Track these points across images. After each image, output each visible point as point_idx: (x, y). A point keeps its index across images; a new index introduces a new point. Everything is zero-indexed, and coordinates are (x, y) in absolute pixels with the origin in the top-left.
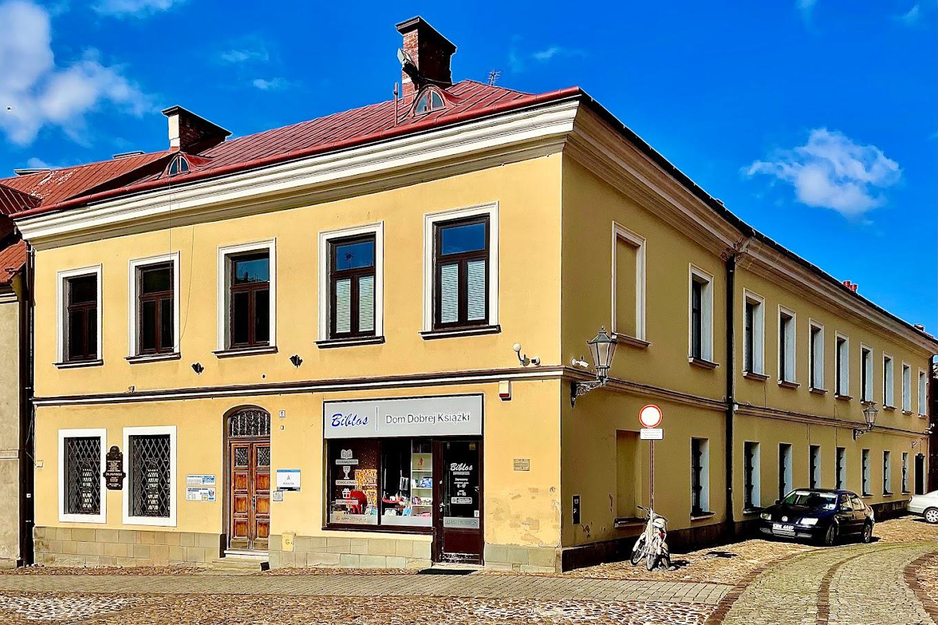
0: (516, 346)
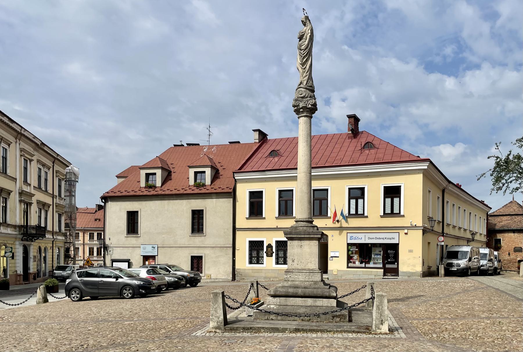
0: (411, 221)
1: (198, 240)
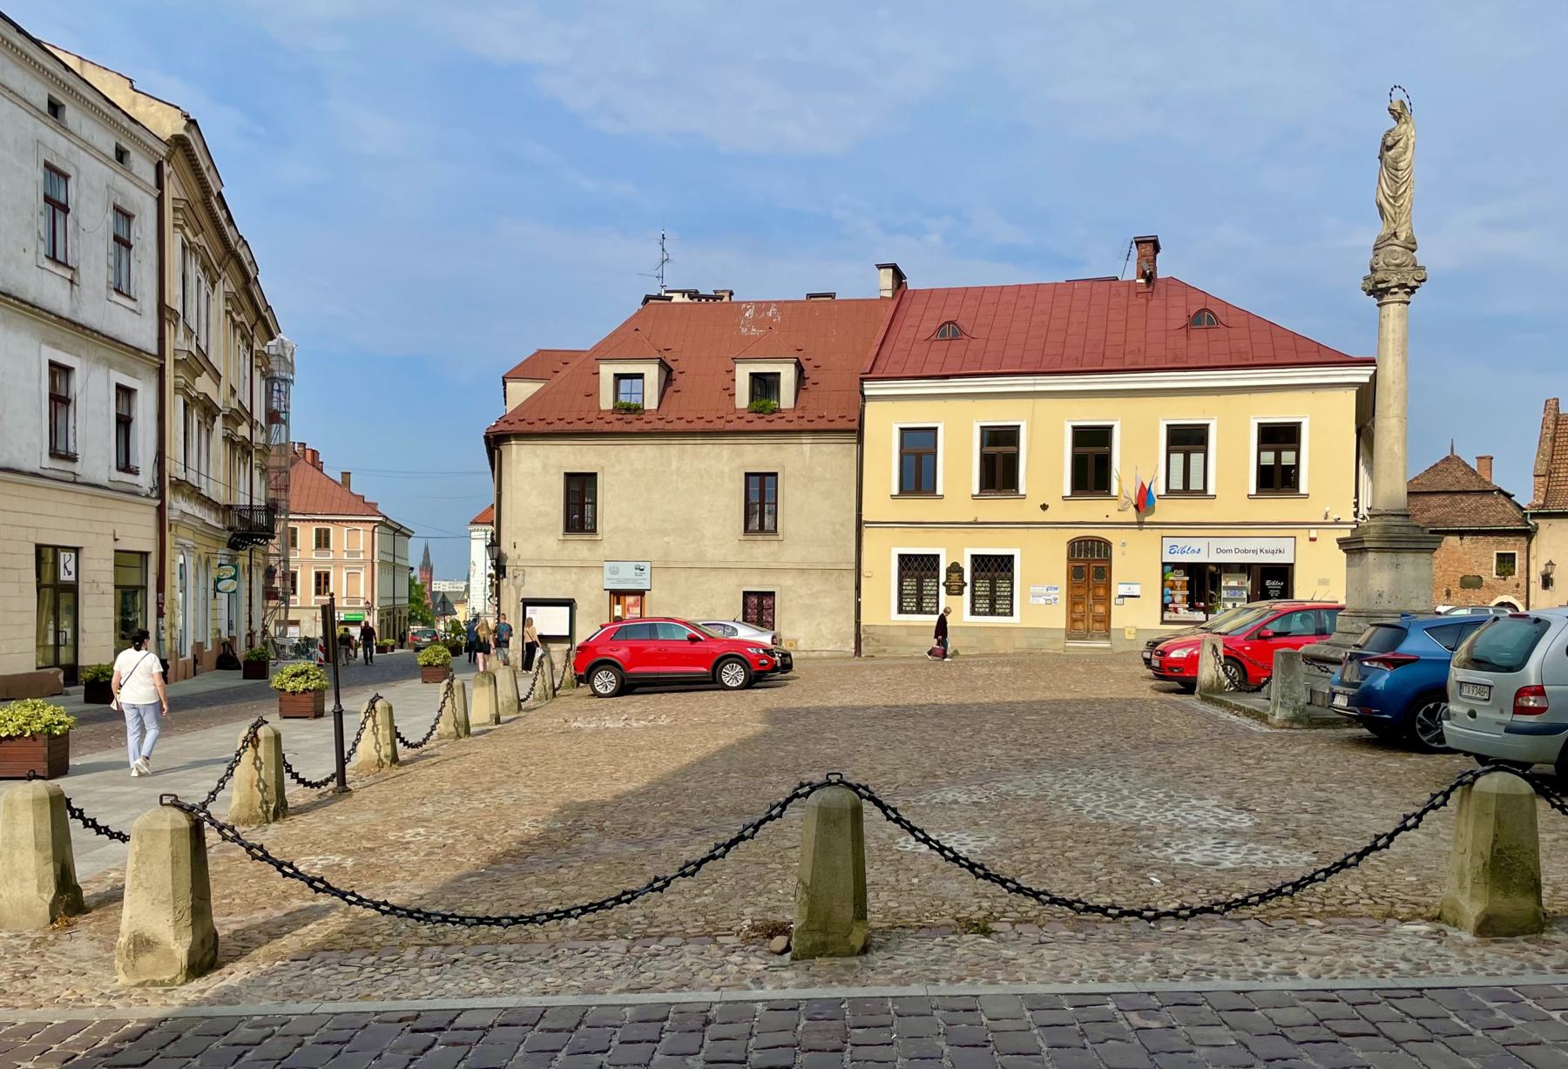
0: (1327, 509)
1: (762, 550)
